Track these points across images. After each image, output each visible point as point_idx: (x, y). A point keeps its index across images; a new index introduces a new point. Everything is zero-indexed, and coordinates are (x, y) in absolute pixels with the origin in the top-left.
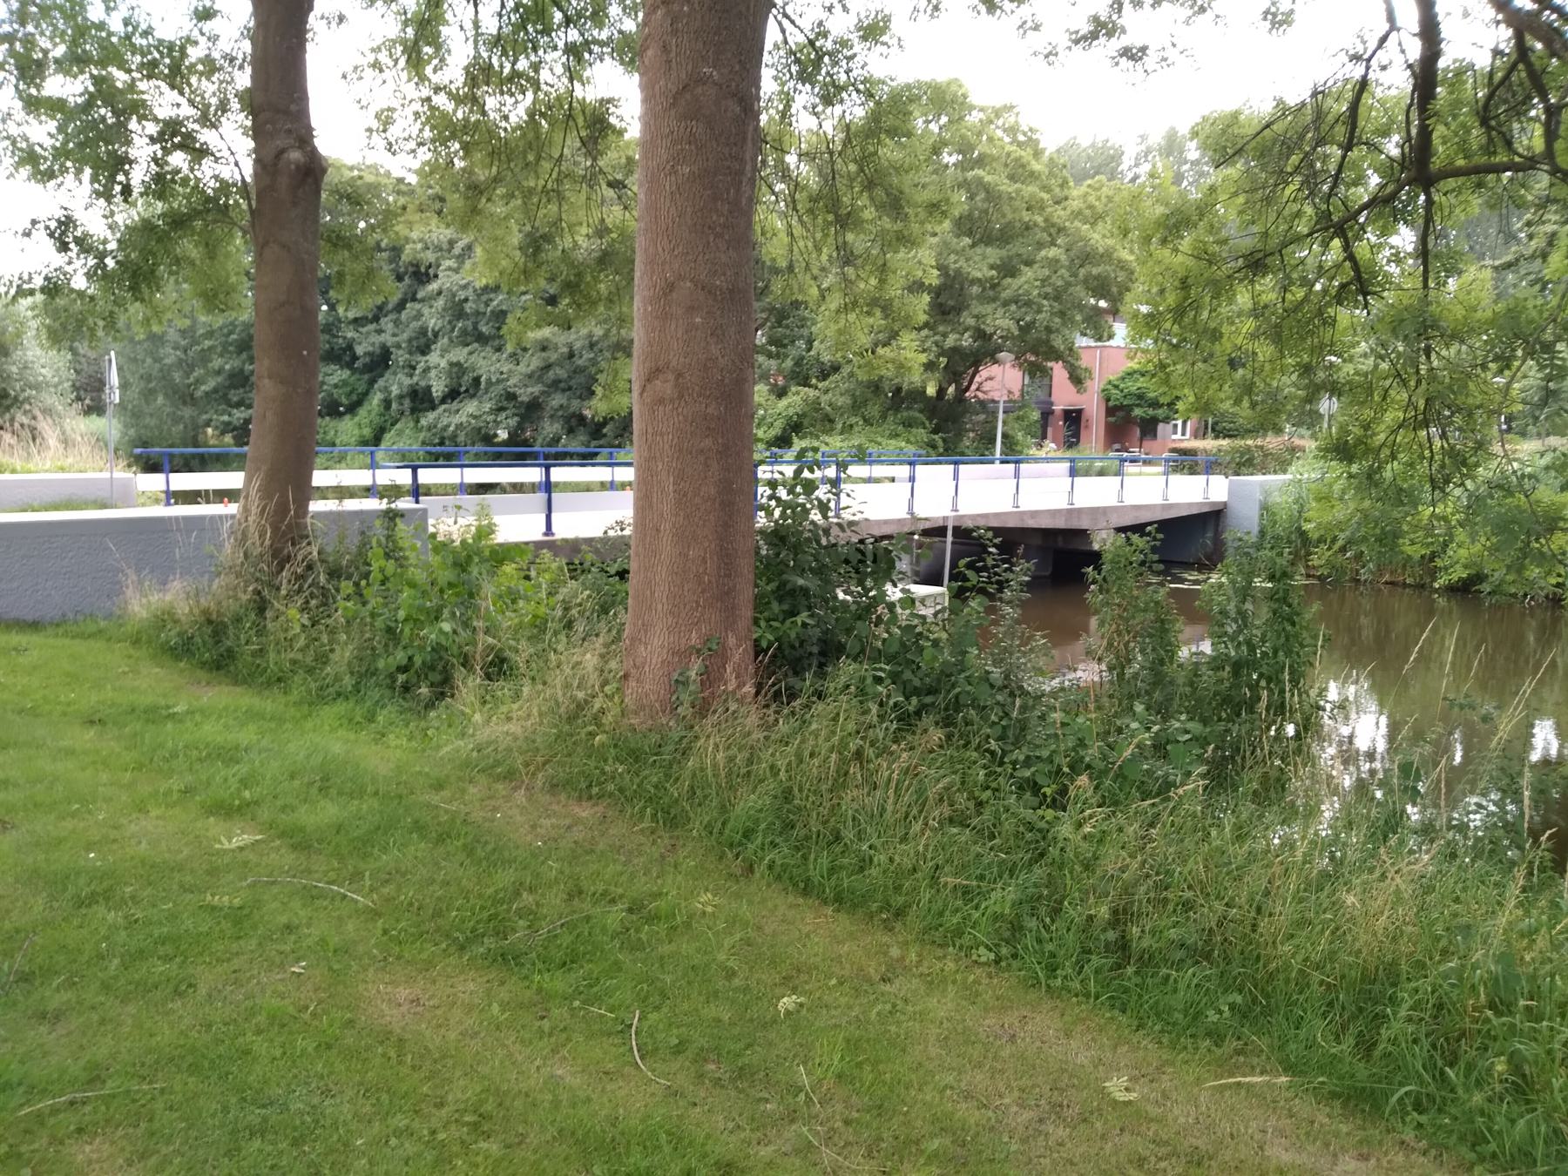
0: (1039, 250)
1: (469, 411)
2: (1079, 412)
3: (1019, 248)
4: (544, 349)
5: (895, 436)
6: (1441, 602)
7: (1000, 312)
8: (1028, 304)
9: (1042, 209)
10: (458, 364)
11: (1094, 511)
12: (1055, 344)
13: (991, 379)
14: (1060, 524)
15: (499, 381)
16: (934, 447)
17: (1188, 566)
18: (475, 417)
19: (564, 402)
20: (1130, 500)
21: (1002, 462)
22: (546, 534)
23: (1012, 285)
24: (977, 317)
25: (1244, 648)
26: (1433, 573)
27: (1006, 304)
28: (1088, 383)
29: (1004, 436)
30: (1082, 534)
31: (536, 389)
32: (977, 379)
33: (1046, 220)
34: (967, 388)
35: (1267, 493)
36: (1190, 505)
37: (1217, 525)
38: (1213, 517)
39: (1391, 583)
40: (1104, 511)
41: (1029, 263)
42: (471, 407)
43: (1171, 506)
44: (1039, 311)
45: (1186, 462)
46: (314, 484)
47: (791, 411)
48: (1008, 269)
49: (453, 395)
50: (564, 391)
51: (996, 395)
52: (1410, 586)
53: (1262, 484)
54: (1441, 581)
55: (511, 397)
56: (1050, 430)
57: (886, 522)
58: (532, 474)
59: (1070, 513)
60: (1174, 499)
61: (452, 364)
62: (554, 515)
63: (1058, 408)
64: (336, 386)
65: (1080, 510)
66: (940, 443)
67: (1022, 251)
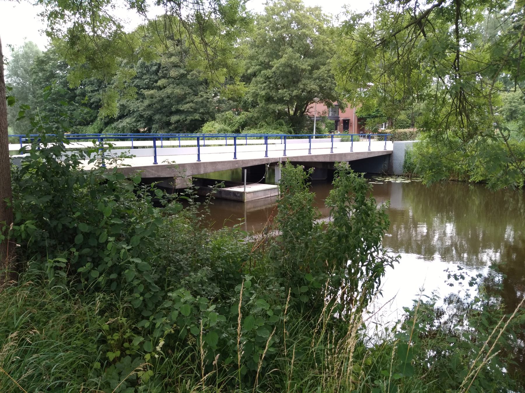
0: (327, 59)
1: (126, 122)
2: (348, 120)
3: (319, 59)
4: (152, 98)
5: (276, 129)
6: (472, 187)
7: (313, 82)
8: (323, 79)
9: (328, 44)
10: (123, 105)
11: (341, 155)
12: (333, 94)
13: (312, 107)
14: (327, 160)
15: (137, 111)
16: (291, 133)
17: (378, 175)
18: (129, 124)
19: (160, 117)
20: (355, 150)
21: (316, 137)
22: (154, 164)
23: (316, 73)
24: (304, 84)
25: (344, 228)
26: (469, 177)
27: (315, 80)
28: (346, 109)
29: (317, 128)
30: (332, 163)
31: (149, 112)
32: (308, 108)
33: (330, 49)
34: (304, 111)
35: (408, 148)
36: (379, 152)
37: (389, 159)
38: (388, 157)
39: (453, 180)
40: (345, 155)
41: (324, 64)
42: (128, 120)
43: (371, 153)
44: (327, 82)
45: (383, 137)
46: (10, 149)
47: (241, 120)
48: (315, 67)
49: (121, 117)
50: (160, 113)
51: (313, 113)
52: (460, 181)
53: (406, 144)
54: (472, 179)
55: (141, 116)
56: (338, 127)
57: (255, 160)
58: (150, 143)
59: (331, 156)
60: (372, 150)
61: (121, 105)
62: (157, 157)
63: (341, 119)
64: (85, 114)
65: (335, 155)
66: (293, 131)
67: (321, 60)
